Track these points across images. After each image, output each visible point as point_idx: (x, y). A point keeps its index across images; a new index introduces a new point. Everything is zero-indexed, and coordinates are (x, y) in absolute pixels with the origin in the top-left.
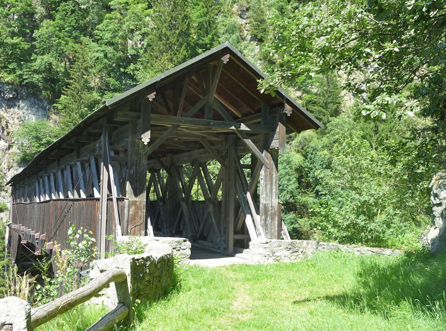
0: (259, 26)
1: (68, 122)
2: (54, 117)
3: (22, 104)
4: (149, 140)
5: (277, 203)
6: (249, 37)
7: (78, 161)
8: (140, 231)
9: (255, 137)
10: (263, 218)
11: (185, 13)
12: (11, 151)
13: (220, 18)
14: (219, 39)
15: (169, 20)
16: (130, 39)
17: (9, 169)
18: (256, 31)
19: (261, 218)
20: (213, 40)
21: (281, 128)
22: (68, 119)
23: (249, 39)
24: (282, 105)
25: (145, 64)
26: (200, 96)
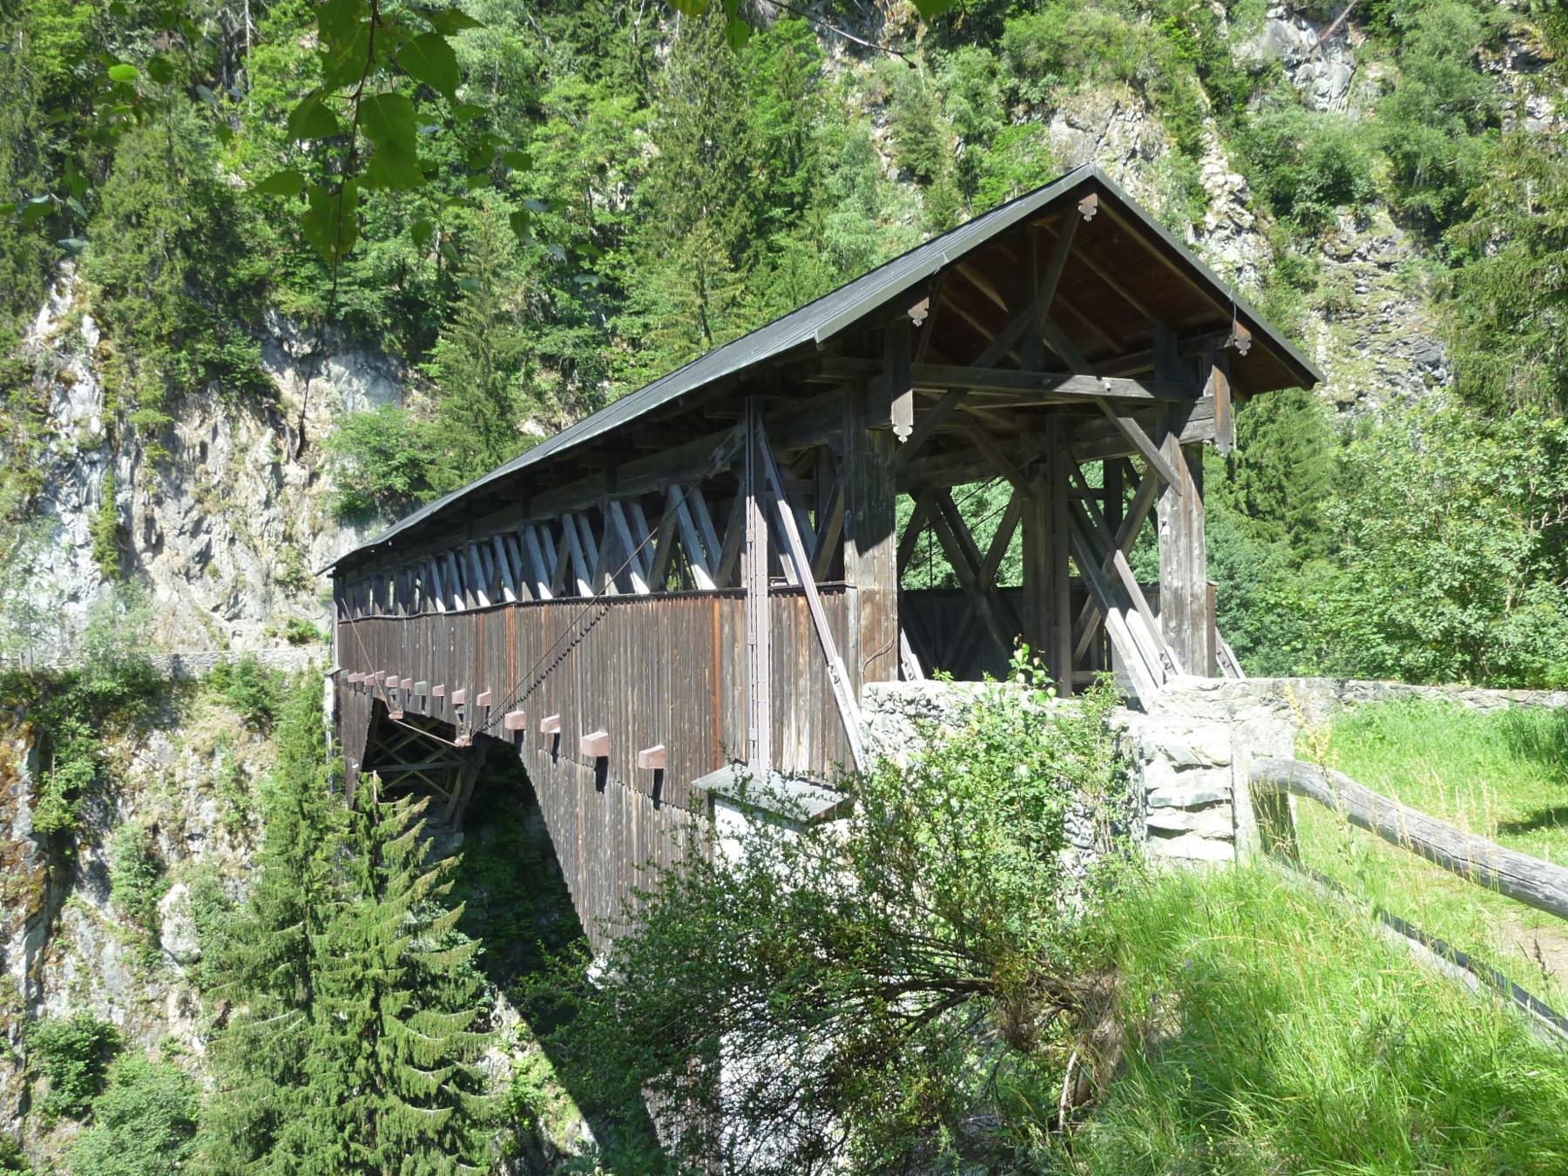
0: (918, 143)
1: (461, 408)
2: (417, 396)
3: (336, 368)
4: (910, 431)
5: (1204, 585)
6: (894, 173)
7: (613, 499)
8: (886, 669)
9: (1141, 413)
10: (1172, 624)
11: (739, 116)
12: (315, 488)
13: (821, 128)
14: (826, 181)
15: (698, 136)
16: (596, 190)
17: (315, 535)
18: (913, 156)
19: (1166, 625)
20: (808, 182)
21: (1216, 384)
22: (456, 399)
23: (895, 177)
24: (1228, 328)
25: (641, 251)
26: (963, 314)
